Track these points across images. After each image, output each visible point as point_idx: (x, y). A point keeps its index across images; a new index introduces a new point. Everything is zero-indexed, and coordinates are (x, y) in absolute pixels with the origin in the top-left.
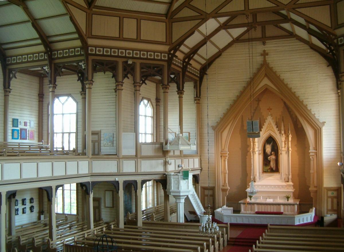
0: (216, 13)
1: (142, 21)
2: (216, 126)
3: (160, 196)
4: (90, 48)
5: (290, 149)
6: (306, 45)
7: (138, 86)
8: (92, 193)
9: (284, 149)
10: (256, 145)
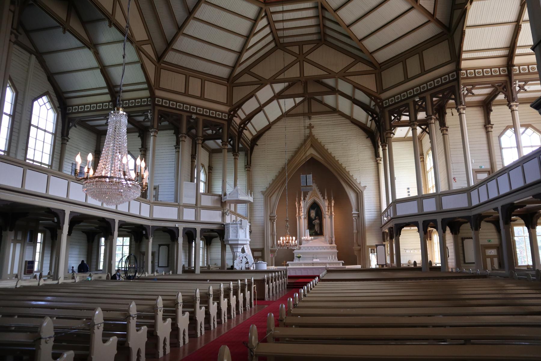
0: (274, 79)
1: (206, 82)
2: (266, 191)
3: (210, 259)
4: (157, 99)
5: (333, 213)
6: (348, 120)
7: (445, 131)
8: (152, 238)
9: (327, 213)
10: (301, 210)
